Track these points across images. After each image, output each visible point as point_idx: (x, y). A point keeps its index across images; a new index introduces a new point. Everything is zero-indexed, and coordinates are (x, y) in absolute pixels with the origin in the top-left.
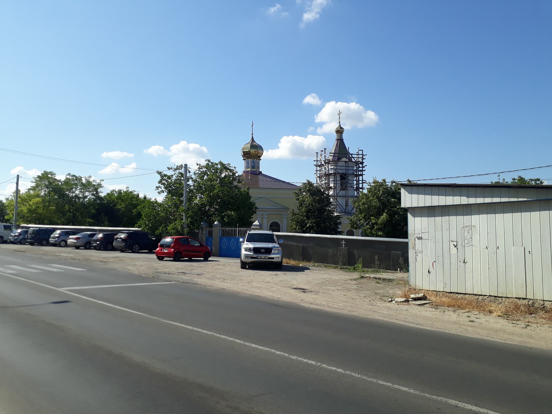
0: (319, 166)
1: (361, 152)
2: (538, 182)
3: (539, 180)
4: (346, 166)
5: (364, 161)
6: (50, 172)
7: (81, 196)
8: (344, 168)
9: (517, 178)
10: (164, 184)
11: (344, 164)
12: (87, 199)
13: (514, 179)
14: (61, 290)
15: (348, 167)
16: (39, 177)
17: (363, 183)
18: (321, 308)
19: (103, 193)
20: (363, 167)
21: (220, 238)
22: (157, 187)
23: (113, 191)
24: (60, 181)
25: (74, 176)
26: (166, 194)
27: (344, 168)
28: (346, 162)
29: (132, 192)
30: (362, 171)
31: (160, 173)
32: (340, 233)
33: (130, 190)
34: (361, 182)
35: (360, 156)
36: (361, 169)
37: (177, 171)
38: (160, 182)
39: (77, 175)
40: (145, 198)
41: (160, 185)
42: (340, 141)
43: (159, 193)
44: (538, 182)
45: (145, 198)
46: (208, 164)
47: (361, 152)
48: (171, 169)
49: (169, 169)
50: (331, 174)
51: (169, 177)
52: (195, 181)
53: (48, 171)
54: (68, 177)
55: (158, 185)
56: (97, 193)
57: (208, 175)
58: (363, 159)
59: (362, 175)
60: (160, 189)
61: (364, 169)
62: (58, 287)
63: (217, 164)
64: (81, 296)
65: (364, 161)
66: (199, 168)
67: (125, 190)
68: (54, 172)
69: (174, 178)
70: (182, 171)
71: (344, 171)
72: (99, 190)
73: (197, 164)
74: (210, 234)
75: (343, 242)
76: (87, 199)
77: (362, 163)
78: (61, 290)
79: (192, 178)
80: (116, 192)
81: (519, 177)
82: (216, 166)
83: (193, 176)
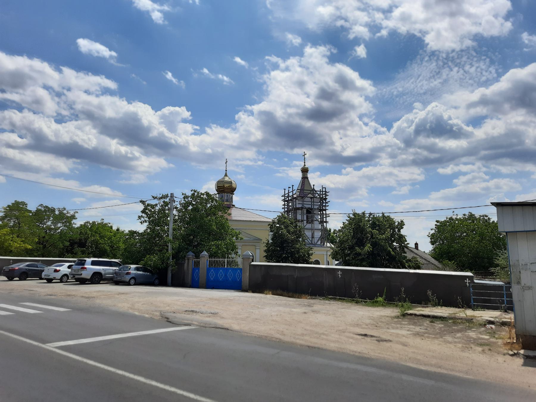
0: (287, 201)
1: (324, 190)
2: (486, 218)
3: (487, 216)
4: (311, 202)
5: (327, 197)
6: (22, 202)
7: (53, 227)
8: (310, 203)
9: (467, 214)
10: (146, 213)
11: (309, 199)
12: (59, 231)
13: (464, 215)
14: (51, 346)
15: (314, 202)
16: (9, 206)
17: (326, 217)
18: (445, 372)
19: (78, 223)
20: (326, 203)
21: (207, 269)
22: (139, 217)
23: (87, 223)
24: (30, 212)
25: (47, 207)
26: (147, 223)
27: (310, 203)
28: (311, 198)
29: (106, 224)
30: (325, 206)
31: (142, 202)
32: (311, 263)
33: (105, 222)
34: (325, 216)
35: (324, 193)
36: (324, 204)
37: (162, 200)
38: (143, 212)
39: (50, 207)
40: (118, 230)
41: (144, 215)
42: (305, 178)
43: (141, 223)
44: (486, 218)
45: (118, 230)
46: (193, 194)
47: (324, 190)
48: (156, 198)
49: (154, 198)
50: (298, 209)
51: (153, 206)
52: (179, 211)
53: (20, 200)
54: (40, 208)
55: (141, 214)
56: (70, 223)
57: (193, 205)
58: (326, 195)
59: (325, 210)
60: (142, 219)
61: (327, 205)
62: (44, 342)
63: (203, 194)
64: (85, 360)
65: (327, 197)
66: (184, 198)
67: (100, 222)
68: (26, 202)
69: (157, 208)
70: (167, 200)
71: (310, 206)
72: (72, 222)
73: (183, 194)
74: (197, 264)
75: (340, 273)
76: (59, 231)
77: (326, 199)
78: (51, 346)
79: (176, 208)
80: (90, 224)
81: (469, 213)
82: (202, 196)
83: (179, 206)
